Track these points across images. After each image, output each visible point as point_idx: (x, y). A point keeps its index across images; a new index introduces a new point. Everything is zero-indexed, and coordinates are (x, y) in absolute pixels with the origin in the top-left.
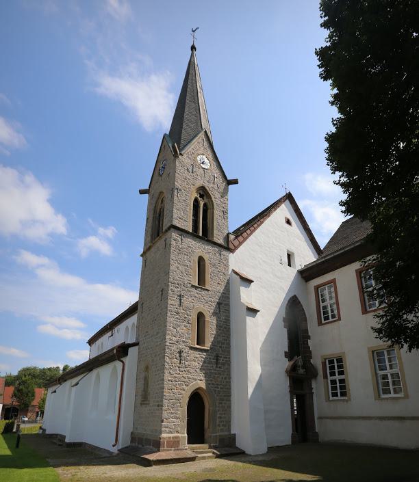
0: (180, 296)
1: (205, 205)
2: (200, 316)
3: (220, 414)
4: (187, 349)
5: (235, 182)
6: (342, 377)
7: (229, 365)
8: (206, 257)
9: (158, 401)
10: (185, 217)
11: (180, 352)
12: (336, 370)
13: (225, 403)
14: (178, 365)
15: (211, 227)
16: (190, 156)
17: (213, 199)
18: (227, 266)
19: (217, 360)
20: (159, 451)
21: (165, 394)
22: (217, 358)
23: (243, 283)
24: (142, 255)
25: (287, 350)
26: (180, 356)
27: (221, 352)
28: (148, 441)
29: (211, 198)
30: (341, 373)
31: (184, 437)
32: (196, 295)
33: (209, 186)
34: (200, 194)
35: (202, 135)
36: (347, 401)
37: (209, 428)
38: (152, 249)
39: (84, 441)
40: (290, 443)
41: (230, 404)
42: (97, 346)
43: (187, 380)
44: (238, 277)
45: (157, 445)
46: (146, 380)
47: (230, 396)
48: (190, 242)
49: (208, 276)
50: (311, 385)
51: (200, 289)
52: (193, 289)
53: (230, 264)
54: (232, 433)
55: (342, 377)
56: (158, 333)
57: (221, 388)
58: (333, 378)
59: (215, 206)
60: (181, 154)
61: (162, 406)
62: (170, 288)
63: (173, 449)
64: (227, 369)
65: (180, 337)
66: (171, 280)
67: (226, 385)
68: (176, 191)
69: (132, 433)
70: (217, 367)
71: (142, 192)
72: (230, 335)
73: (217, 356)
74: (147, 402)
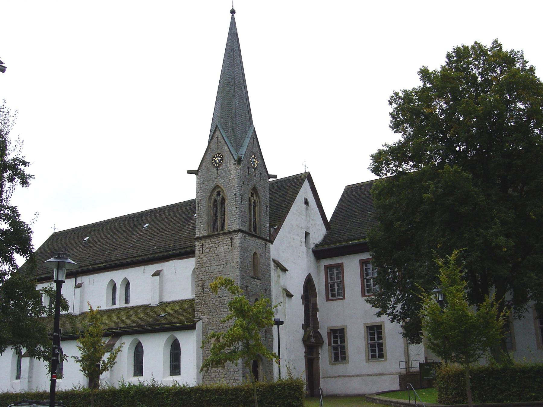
12: (339, 339)
25: (304, 323)
50: (318, 352)
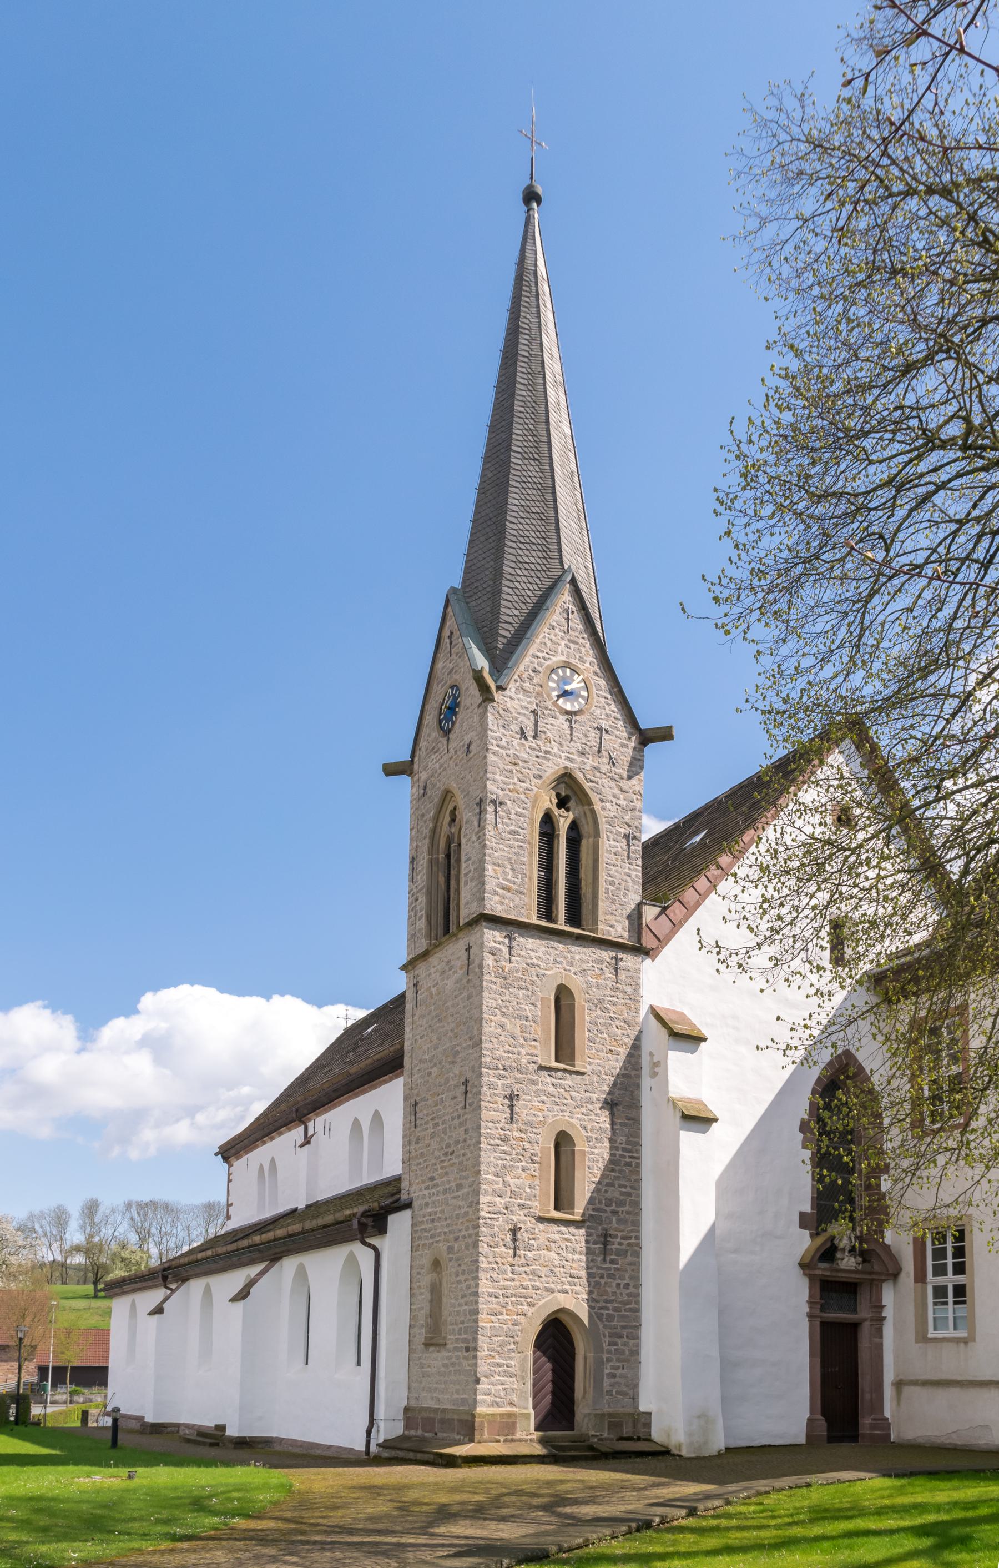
0: (511, 1097)
1: (574, 826)
2: (563, 1142)
3: (612, 1367)
4: (530, 1223)
5: (665, 734)
6: (960, 1279)
7: (637, 1254)
8: (576, 984)
9: (465, 1340)
10: (518, 881)
11: (514, 1231)
13: (625, 1344)
14: (510, 1259)
15: (589, 896)
16: (527, 685)
17: (597, 806)
18: (635, 999)
19: (605, 1244)
20: (472, 1440)
21: (480, 1324)
22: (605, 1238)
23: (672, 1041)
24: (404, 968)
25: (807, 1208)
26: (515, 1240)
27: (614, 1224)
28: (446, 1423)
29: (590, 803)
30: (960, 1269)
31: (527, 1416)
32: (551, 1089)
33: (583, 768)
34: (558, 795)
35: (564, 598)
36: (965, 1341)
37: (584, 1397)
38: (434, 960)
39: (274, 1435)
40: (802, 1439)
41: (638, 1345)
42: (254, 1168)
43: (531, 1292)
44: (664, 1032)
45: (468, 1429)
46: (436, 1291)
47: (638, 1327)
48: (530, 946)
49: (582, 1035)
51: (560, 1074)
52: (544, 1077)
53: (643, 991)
54: (642, 1408)
55: (960, 1279)
56: (459, 1187)
57: (615, 1310)
58: (940, 1280)
59: (603, 826)
60: (499, 688)
61: (475, 1349)
62: (485, 1079)
63: (502, 1439)
64: (631, 1264)
65: (514, 1195)
66: (486, 1060)
67: (629, 1303)
68: (490, 809)
69: (407, 1409)
70: (604, 1260)
71: (391, 770)
72: (639, 1181)
73: (606, 1235)
74: (442, 1342)
